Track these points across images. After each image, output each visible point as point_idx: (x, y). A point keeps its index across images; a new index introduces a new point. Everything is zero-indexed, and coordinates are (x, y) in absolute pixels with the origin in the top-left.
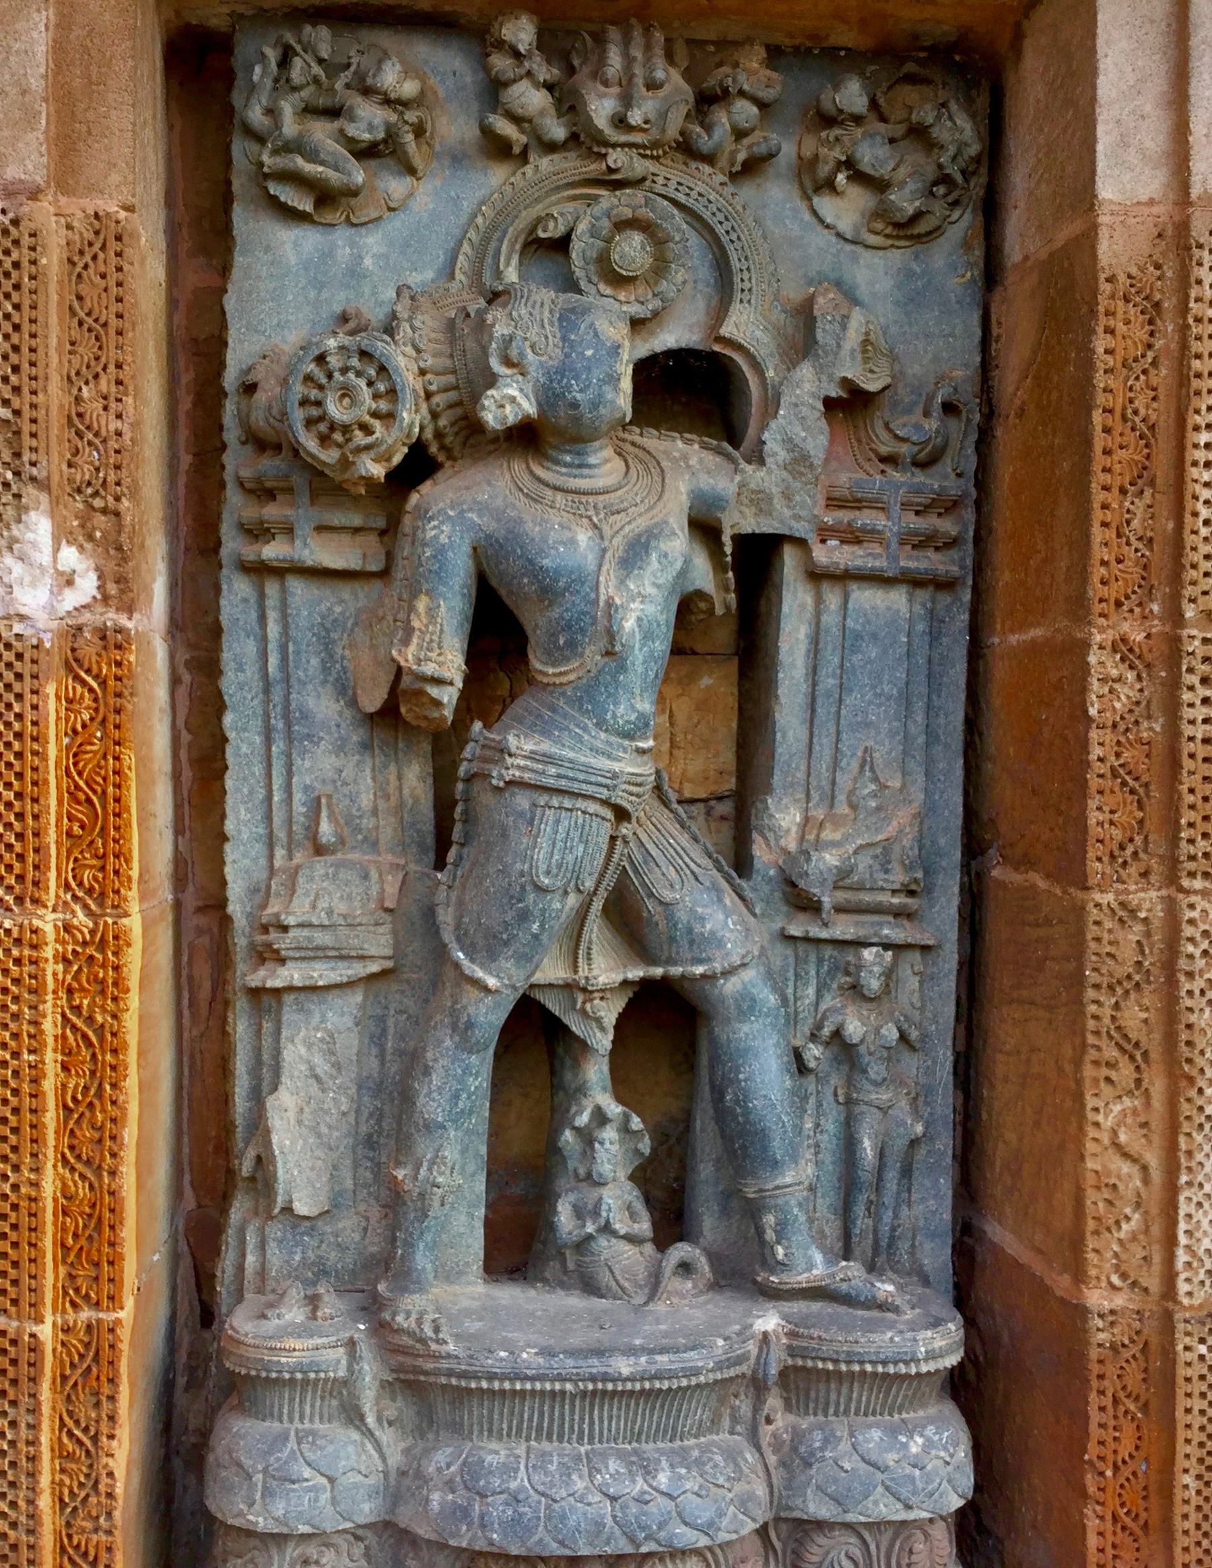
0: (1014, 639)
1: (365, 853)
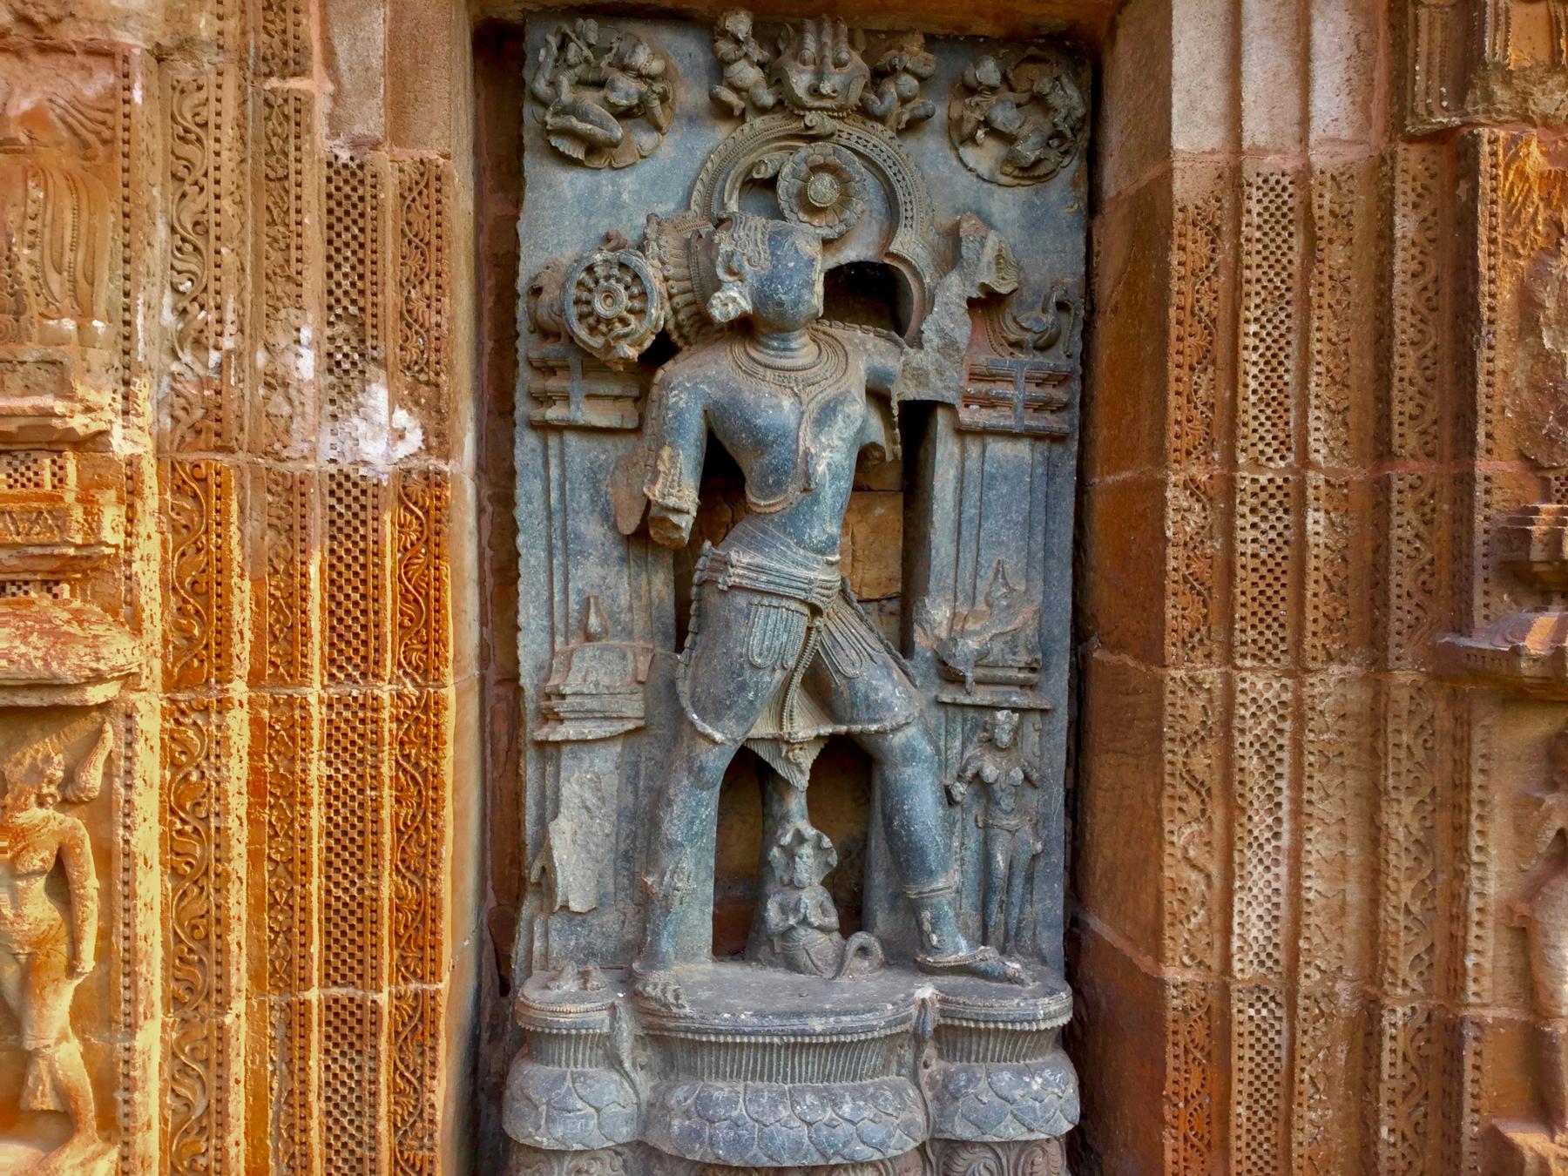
0: (1110, 479)
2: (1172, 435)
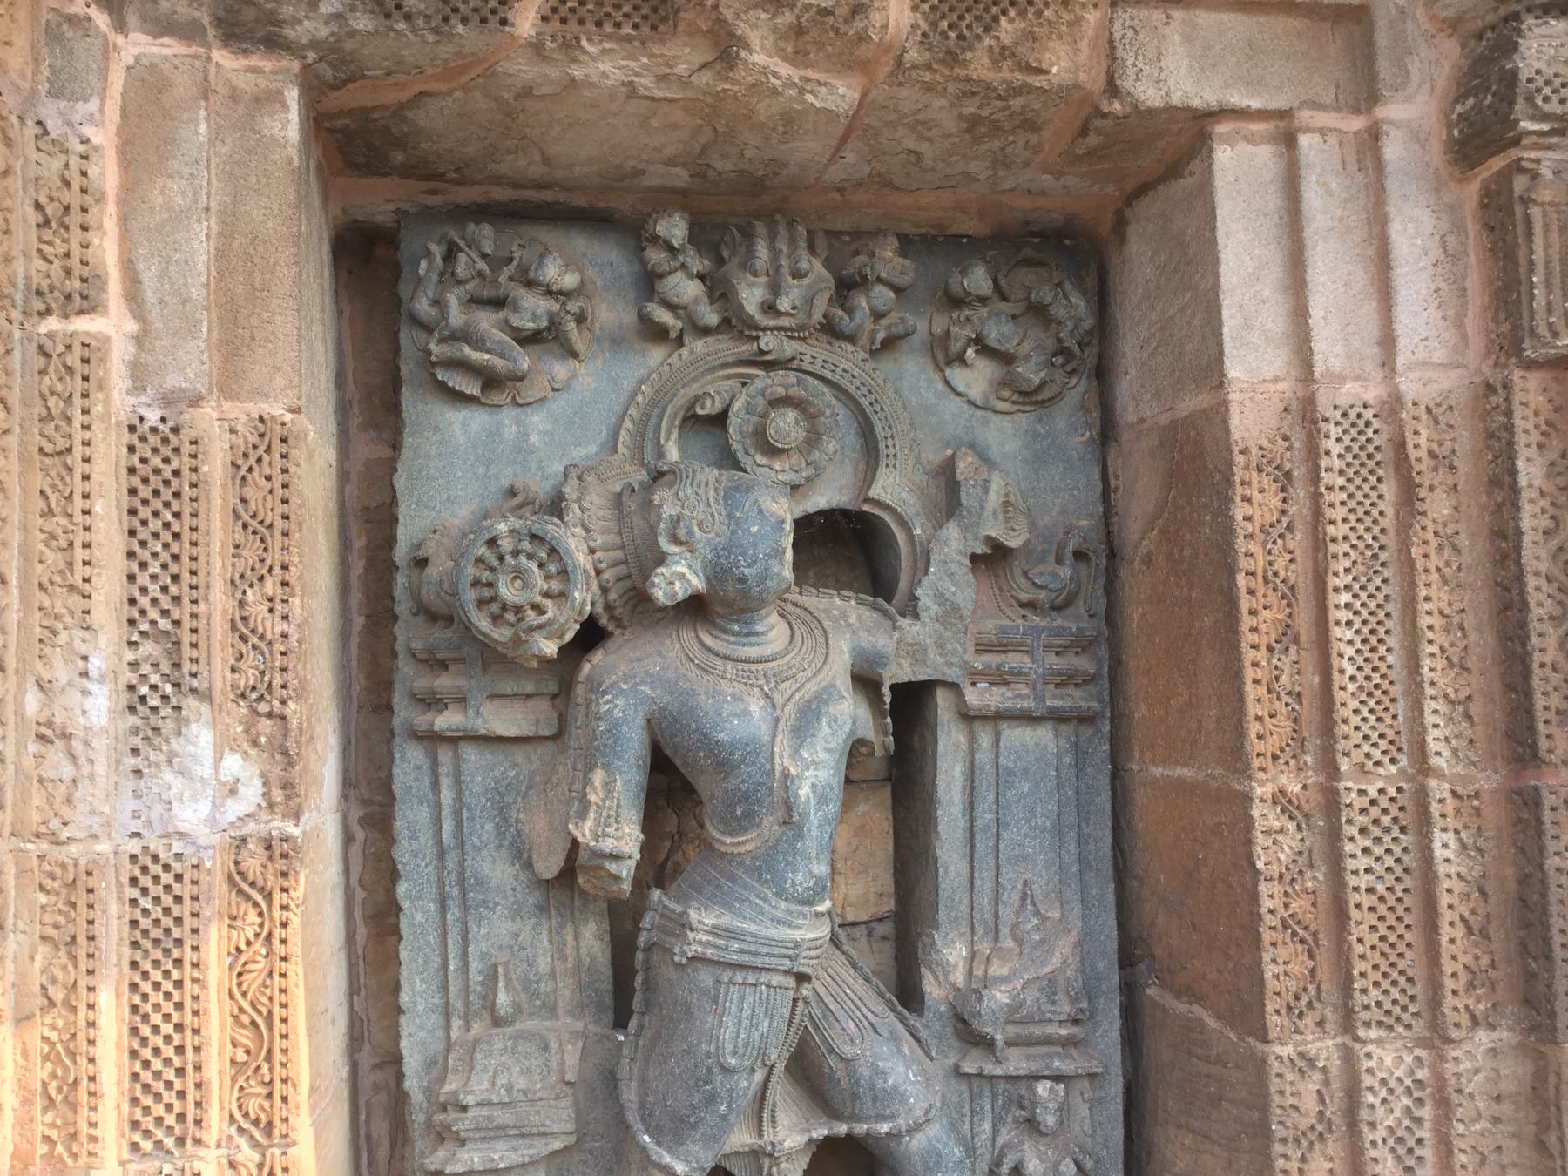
0: (1157, 771)
1: (543, 1019)
2: (1253, 736)
